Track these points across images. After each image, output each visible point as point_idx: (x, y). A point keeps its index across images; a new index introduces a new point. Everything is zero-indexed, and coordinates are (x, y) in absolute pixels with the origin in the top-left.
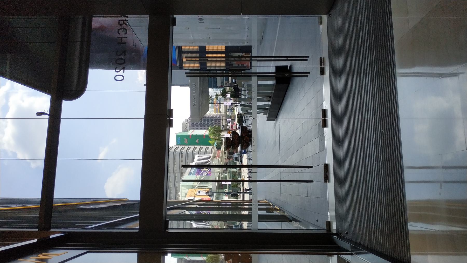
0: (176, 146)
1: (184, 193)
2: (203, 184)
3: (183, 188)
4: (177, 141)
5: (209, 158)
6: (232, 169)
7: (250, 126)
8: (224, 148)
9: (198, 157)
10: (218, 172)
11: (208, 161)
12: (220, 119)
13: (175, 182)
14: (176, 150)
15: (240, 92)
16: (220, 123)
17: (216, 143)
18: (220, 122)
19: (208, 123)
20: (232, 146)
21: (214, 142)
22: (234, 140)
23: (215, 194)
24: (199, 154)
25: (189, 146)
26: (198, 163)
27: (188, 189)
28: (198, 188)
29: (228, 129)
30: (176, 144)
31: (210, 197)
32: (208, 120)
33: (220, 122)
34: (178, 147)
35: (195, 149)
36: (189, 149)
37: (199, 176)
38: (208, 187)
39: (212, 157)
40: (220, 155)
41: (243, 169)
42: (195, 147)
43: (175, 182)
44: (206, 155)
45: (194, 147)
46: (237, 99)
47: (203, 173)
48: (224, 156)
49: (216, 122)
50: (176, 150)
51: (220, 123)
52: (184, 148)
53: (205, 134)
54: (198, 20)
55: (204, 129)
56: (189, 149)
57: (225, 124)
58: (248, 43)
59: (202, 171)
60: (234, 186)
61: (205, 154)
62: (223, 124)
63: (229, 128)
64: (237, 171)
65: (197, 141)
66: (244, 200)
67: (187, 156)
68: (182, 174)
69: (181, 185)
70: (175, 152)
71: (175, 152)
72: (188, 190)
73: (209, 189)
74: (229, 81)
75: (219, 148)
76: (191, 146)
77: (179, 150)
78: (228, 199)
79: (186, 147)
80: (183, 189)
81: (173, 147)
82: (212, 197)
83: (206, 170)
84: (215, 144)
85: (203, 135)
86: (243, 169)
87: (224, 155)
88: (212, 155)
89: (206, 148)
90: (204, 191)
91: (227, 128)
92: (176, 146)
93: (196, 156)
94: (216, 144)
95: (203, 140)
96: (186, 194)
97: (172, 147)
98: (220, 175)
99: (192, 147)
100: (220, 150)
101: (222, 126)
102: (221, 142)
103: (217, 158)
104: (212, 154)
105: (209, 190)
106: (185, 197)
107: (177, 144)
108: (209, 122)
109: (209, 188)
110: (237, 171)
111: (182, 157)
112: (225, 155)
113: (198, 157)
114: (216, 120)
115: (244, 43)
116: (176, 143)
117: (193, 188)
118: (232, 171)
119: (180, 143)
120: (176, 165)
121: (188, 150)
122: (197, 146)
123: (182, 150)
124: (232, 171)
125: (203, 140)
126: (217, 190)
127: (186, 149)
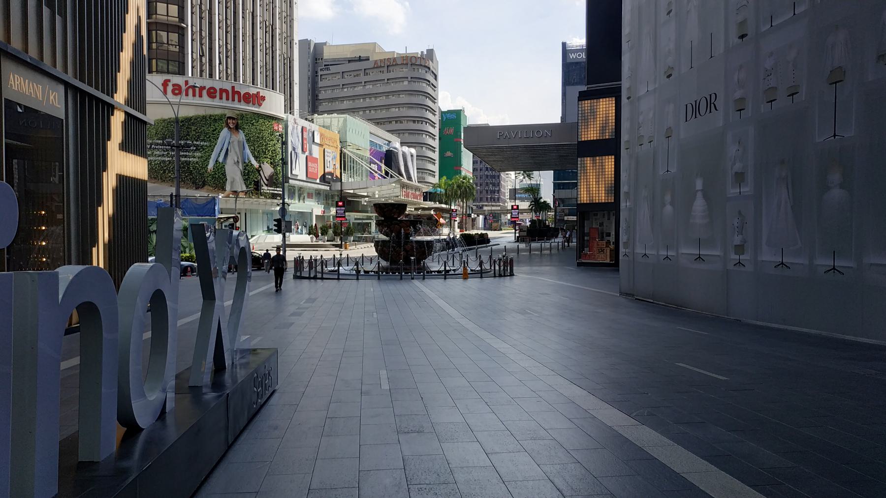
0: (437, 110)
1: (331, 124)
2: (349, 164)
3: (342, 120)
4: (449, 112)
5: (409, 178)
6: (374, 223)
7: (492, 261)
8: (427, 207)
9: (412, 156)
10: (374, 194)
11: (401, 175)
12: (496, 200)
13: (364, 109)
14: (429, 110)
15: (538, 241)
16: (487, 200)
17: (441, 192)
18: (489, 199)
19: (487, 176)
20: (383, 219)
21: (443, 187)
22: (398, 224)
23: (328, 188)
24: (417, 156)
25: (437, 138)
26: (397, 153)
27: (339, 132)
28: (341, 154)
29: (471, 217)
30: (443, 110)
31: (319, 177)
32: (493, 177)
33: (489, 199)
34: (435, 115)
35: (432, 149)
36: (432, 136)
37: (369, 156)
38: (343, 174)
39: (410, 182)
40: (410, 199)
41: (371, 246)
42: (436, 150)
43: (364, 109)
44: (416, 171)
45: (435, 148)
46: (525, 234)
47: (375, 163)
48: (411, 208)
49: (489, 192)
50: (429, 110)
51: (487, 200)
52: (432, 126)
53: (462, 169)
54: (696, 101)
55: (474, 170)
56: (432, 136)
57: (485, 211)
58: (626, 258)
59: (381, 162)
60: (336, 227)
61: (417, 169)
62: (486, 206)
63: (473, 217)
64: (370, 234)
65: (449, 154)
66: (287, 249)
67: (415, 133)
68: (378, 123)
69: (347, 115)
70: (424, 108)
71: (424, 108)
72: (337, 132)
73: (339, 177)
74: (569, 217)
75: (428, 196)
76: (437, 141)
77: (430, 116)
78: (316, 216)
79: (436, 131)
80: (338, 121)
81: (435, 103)
82: (320, 181)
83: (383, 172)
84: (439, 189)
85: (460, 166)
86: (371, 246)
87: (412, 208)
88: (415, 182)
89: (434, 172)
90: (335, 165)
91: (473, 215)
92: (437, 110)
93: (413, 151)
94: (438, 192)
95: (450, 165)
96: (328, 127)
97: (435, 101)
98: (367, 199)
99: (436, 143)
100: (422, 199)
101: (483, 205)
102: (444, 201)
103: (404, 193)
104: (417, 184)
105: (336, 176)
106: (322, 125)
107: (443, 113)
108: (489, 177)
109: (343, 177)
110: (370, 234)
111: (414, 122)
112: (413, 210)
113: (412, 156)
114: (493, 192)
115: (626, 245)
116: (446, 110)
117: (340, 142)
118: (370, 223)
119: (445, 118)
120: (399, 110)
121: (429, 135)
122: (437, 153)
123: (429, 123)
124: (370, 223)
125: (450, 165)
126: (338, 192)
127: (431, 129)
